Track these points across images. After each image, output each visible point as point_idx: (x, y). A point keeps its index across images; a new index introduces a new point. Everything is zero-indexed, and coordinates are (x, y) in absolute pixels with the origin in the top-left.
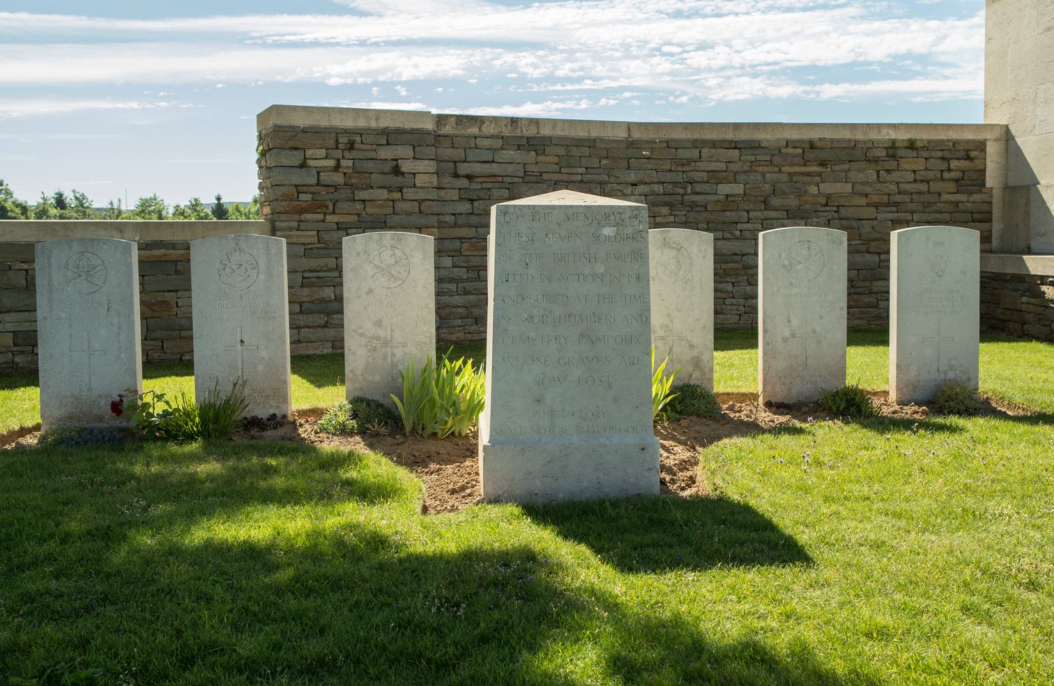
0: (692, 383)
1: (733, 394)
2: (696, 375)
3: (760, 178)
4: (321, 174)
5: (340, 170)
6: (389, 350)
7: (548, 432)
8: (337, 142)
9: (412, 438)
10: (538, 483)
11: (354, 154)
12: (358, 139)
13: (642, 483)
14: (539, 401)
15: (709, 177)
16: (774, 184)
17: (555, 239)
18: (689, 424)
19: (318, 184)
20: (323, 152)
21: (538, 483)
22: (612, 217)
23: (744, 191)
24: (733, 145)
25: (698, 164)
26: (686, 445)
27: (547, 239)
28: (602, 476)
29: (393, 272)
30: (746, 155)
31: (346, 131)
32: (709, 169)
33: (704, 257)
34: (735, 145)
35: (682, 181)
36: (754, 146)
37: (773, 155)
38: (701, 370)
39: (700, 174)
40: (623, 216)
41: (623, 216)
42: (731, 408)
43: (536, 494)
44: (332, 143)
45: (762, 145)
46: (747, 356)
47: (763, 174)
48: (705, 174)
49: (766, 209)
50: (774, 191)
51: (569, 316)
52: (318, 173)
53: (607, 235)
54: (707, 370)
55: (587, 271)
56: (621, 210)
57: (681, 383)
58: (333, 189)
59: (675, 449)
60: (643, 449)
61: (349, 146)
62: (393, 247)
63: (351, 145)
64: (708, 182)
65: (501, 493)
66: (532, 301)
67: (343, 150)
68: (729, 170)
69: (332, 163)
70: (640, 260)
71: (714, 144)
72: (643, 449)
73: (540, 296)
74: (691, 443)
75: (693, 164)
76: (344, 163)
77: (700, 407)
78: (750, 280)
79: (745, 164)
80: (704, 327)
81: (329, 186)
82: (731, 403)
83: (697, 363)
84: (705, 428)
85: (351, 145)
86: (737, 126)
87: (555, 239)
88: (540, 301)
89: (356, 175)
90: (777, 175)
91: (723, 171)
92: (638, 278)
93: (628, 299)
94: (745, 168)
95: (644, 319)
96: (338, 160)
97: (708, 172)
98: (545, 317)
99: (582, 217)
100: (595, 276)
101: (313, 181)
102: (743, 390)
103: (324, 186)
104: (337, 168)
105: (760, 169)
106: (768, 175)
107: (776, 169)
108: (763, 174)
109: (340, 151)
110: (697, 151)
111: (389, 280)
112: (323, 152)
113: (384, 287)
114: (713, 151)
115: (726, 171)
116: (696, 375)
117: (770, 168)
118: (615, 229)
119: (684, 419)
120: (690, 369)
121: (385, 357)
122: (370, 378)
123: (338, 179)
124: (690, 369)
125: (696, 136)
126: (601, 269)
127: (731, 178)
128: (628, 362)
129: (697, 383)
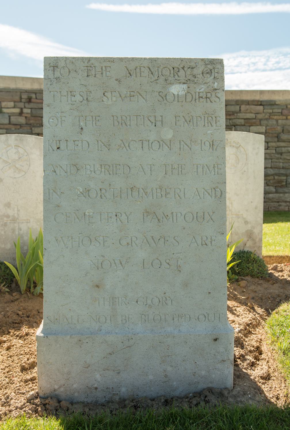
0: (246, 249)
1: (273, 257)
2: (249, 244)
3: (275, 123)
4: (12, 117)
5: (23, 115)
6: (16, 225)
7: (108, 321)
8: (21, 98)
9: (25, 295)
10: (98, 377)
11: (31, 105)
12: (34, 96)
13: (214, 376)
14: (98, 286)
15: (245, 122)
16: (283, 126)
17: (114, 99)
18: (247, 285)
19: (10, 123)
20: (12, 104)
21: (98, 377)
22: (182, 73)
23: (266, 130)
24: (259, 103)
25: (239, 114)
26: (246, 305)
27: (105, 99)
28: (169, 369)
29: (17, 166)
30: (267, 109)
31: (26, 91)
32: (245, 117)
33: (257, 154)
34: (260, 103)
35: (229, 124)
36: (271, 104)
37: (282, 109)
38: (253, 240)
39: (240, 120)
40: (195, 71)
41: (195, 71)
42: (275, 269)
43: (96, 388)
44: (17, 98)
45: (277, 103)
46: (273, 228)
47: (277, 121)
48: (243, 121)
49: (278, 141)
50: (283, 130)
51: (132, 189)
52: (10, 116)
53: (176, 93)
54: (257, 240)
55: (152, 137)
56: (193, 65)
57: (238, 250)
58: (19, 127)
59: (238, 309)
60: (216, 340)
61: (28, 100)
62: (17, 146)
63: (29, 100)
64: (244, 125)
65: (56, 387)
66: (89, 172)
67: (24, 103)
68: (257, 118)
69: (17, 111)
70: (214, 124)
71: (248, 103)
72: (216, 340)
73: (98, 166)
74: (251, 304)
75: (236, 114)
76: (25, 111)
77: (254, 270)
78: (268, 183)
79: (266, 114)
80: (256, 208)
81: (16, 125)
82: (275, 264)
83: (250, 235)
84: (259, 288)
85: (29, 100)
86: (262, 92)
87: (114, 99)
88: (98, 172)
89: (32, 118)
90: (284, 121)
91: (253, 119)
92: (212, 145)
93: (200, 170)
94: (267, 117)
95: (219, 194)
96: (22, 109)
97: (245, 119)
98: (103, 191)
99: (146, 72)
100: (161, 142)
101: (7, 121)
102: (281, 254)
103: (14, 125)
104: (21, 114)
105: (275, 117)
106: (280, 121)
107: (285, 117)
108: (277, 121)
109: (23, 104)
110: (238, 107)
111: (15, 172)
112: (12, 104)
113: (11, 177)
114: (248, 107)
115: (255, 119)
116: (249, 244)
117: (281, 117)
118: (185, 86)
119: (242, 279)
120: (245, 239)
121: (13, 230)
122: (3, 246)
123: (22, 120)
124: (245, 239)
125: (238, 98)
126: (168, 134)
127: (258, 123)
128: (199, 242)
129: (250, 250)
